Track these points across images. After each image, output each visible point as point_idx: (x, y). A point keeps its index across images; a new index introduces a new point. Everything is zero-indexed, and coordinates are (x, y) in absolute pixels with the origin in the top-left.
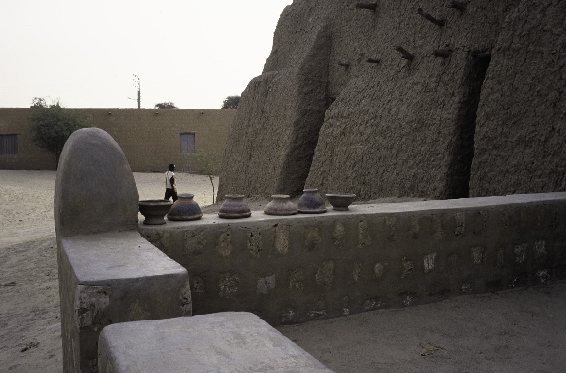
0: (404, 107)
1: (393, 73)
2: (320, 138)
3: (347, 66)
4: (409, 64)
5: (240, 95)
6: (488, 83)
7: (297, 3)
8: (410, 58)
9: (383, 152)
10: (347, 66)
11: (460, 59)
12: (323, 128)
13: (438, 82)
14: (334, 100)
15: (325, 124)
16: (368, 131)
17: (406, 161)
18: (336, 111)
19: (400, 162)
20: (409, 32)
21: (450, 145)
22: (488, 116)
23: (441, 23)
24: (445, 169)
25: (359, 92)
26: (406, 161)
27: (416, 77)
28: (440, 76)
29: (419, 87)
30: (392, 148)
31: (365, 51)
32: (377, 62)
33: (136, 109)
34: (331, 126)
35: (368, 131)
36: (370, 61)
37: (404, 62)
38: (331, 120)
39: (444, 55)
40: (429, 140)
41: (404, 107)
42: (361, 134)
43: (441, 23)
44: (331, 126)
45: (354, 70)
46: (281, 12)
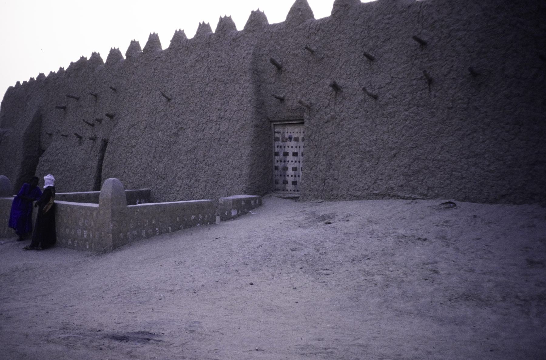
0: (77, 159)
1: (73, 143)
2: (37, 171)
3: (51, 135)
4: (80, 141)
5: (14, 86)
6: (106, 155)
7: (250, 31)
8: (81, 138)
9: (69, 179)
10: (51, 135)
11: (99, 142)
12: (38, 166)
13: (91, 150)
14: (44, 151)
15: (39, 164)
16: (62, 169)
17: (78, 183)
18: (46, 158)
19: (76, 183)
20: (80, 125)
21: (95, 176)
22: (106, 166)
23: (93, 125)
24: (93, 186)
25: (57, 150)
26: (78, 183)
27: (83, 146)
28: (92, 148)
29: (84, 151)
30: (72, 177)
31: (60, 128)
32: (66, 136)
33: (236, 30)
34: (43, 165)
35: (62, 169)
36: (63, 135)
37: (78, 139)
38: (43, 163)
39: (94, 139)
40: (87, 174)
41: (77, 159)
42: (58, 171)
43: (93, 125)
44: (43, 165)
45: (54, 137)
46: (288, 10)
